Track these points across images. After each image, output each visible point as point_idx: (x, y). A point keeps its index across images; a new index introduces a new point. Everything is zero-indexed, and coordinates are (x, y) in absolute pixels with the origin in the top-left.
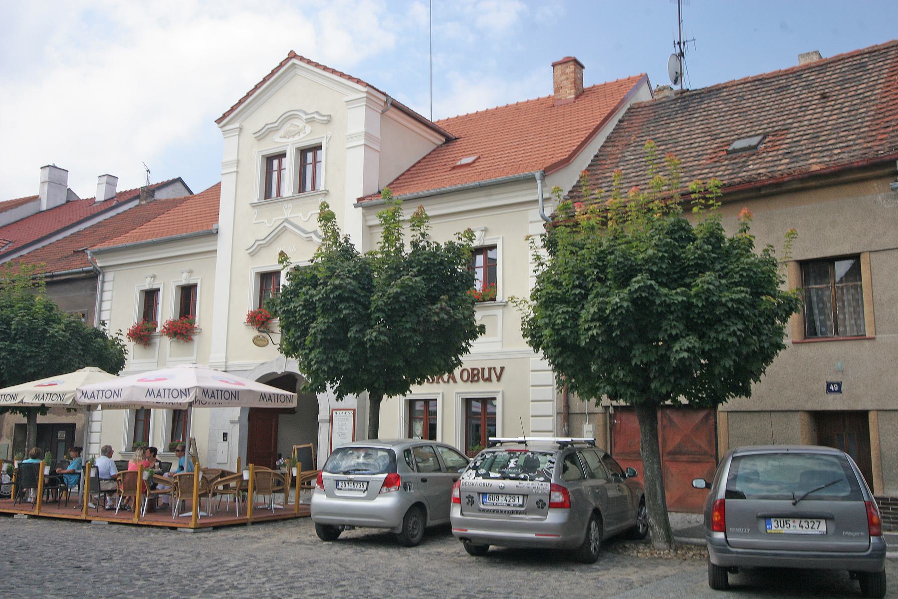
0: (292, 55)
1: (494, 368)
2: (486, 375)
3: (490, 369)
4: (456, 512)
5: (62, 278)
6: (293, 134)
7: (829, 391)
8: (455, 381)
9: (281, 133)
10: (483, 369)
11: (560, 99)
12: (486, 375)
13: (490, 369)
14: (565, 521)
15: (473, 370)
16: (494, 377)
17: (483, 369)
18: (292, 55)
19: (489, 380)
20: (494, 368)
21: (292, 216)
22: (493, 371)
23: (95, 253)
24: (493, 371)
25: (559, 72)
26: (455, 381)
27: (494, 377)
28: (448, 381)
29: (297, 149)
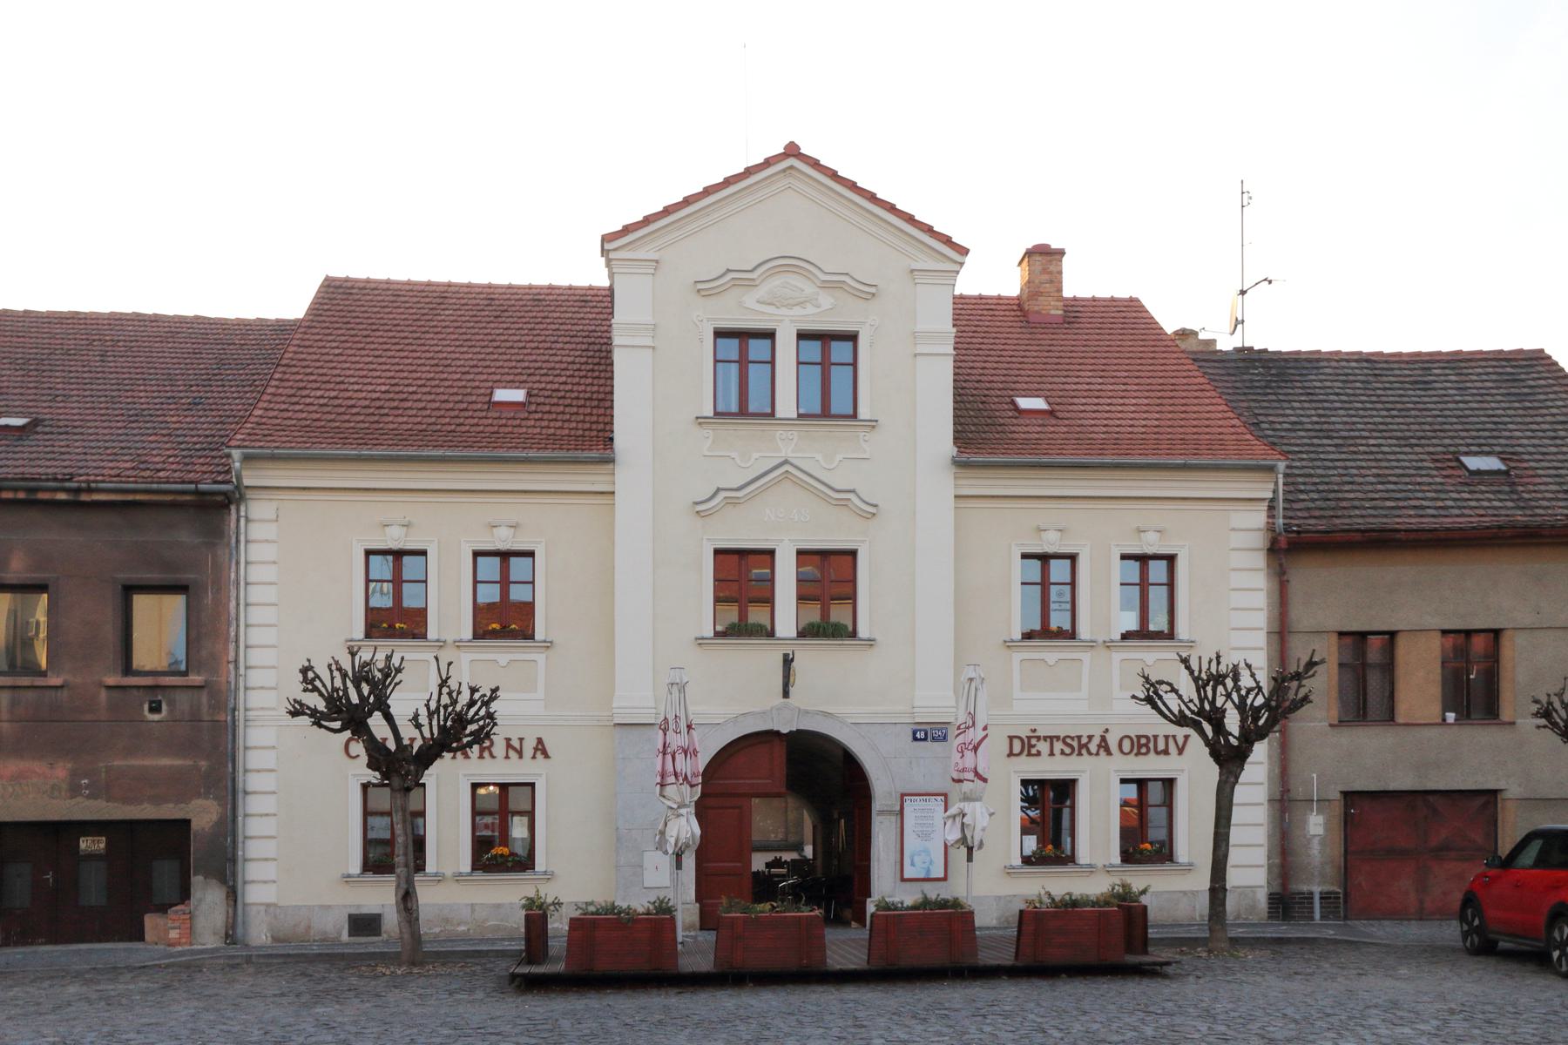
0: (792, 151)
1: (1174, 737)
2: (1161, 746)
3: (1167, 737)
4: (977, 933)
5: (139, 497)
6: (791, 301)
7: (915, 739)
8: (1109, 753)
9: (762, 292)
10: (1156, 737)
11: (1038, 312)
12: (1161, 746)
13: (1167, 737)
14: (214, 881)
15: (1139, 737)
16: (1172, 748)
17: (1156, 737)
18: (792, 151)
19: (1166, 752)
20: (1174, 737)
21: (794, 455)
22: (1171, 741)
23: (247, 458)
24: (1171, 741)
25: (1038, 268)
26: (1109, 753)
27: (1172, 748)
28: (1097, 754)
29: (858, 332)
